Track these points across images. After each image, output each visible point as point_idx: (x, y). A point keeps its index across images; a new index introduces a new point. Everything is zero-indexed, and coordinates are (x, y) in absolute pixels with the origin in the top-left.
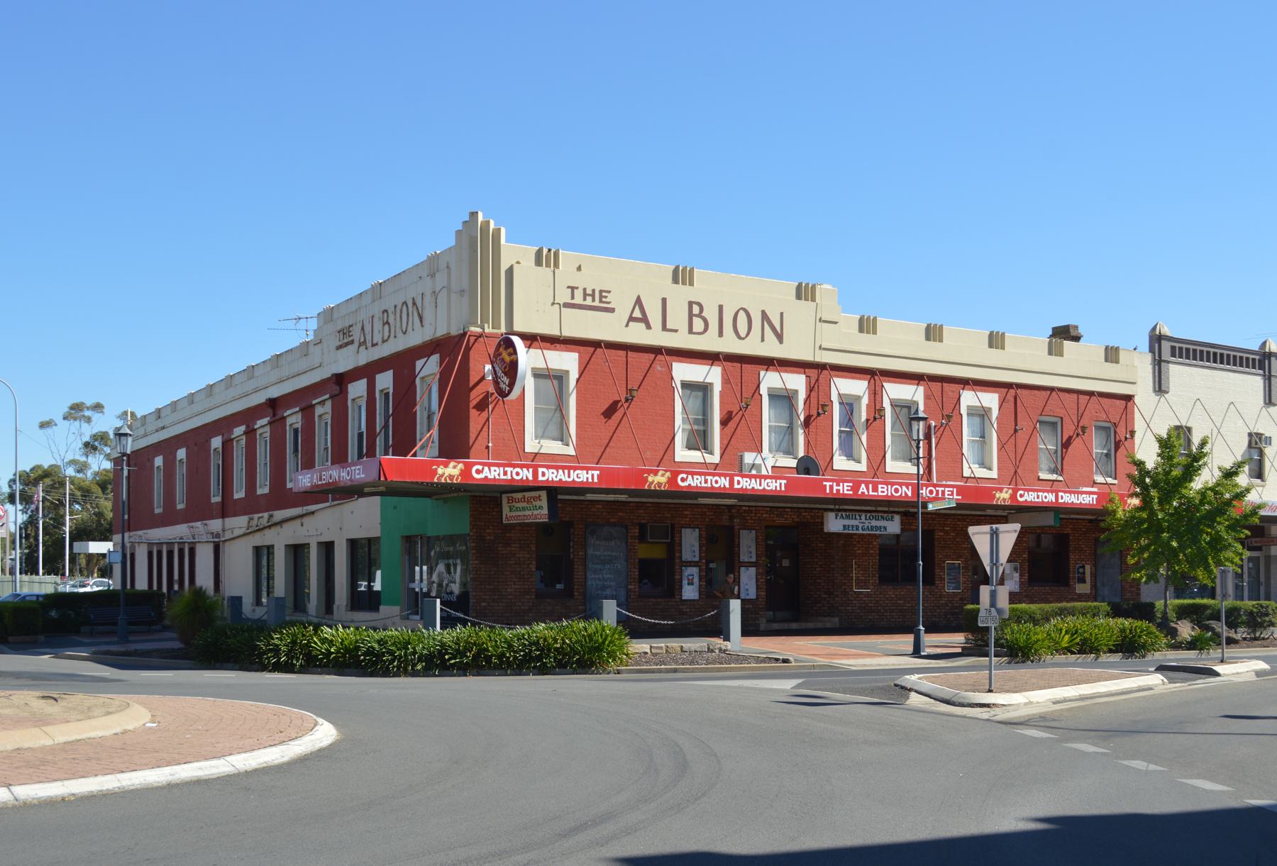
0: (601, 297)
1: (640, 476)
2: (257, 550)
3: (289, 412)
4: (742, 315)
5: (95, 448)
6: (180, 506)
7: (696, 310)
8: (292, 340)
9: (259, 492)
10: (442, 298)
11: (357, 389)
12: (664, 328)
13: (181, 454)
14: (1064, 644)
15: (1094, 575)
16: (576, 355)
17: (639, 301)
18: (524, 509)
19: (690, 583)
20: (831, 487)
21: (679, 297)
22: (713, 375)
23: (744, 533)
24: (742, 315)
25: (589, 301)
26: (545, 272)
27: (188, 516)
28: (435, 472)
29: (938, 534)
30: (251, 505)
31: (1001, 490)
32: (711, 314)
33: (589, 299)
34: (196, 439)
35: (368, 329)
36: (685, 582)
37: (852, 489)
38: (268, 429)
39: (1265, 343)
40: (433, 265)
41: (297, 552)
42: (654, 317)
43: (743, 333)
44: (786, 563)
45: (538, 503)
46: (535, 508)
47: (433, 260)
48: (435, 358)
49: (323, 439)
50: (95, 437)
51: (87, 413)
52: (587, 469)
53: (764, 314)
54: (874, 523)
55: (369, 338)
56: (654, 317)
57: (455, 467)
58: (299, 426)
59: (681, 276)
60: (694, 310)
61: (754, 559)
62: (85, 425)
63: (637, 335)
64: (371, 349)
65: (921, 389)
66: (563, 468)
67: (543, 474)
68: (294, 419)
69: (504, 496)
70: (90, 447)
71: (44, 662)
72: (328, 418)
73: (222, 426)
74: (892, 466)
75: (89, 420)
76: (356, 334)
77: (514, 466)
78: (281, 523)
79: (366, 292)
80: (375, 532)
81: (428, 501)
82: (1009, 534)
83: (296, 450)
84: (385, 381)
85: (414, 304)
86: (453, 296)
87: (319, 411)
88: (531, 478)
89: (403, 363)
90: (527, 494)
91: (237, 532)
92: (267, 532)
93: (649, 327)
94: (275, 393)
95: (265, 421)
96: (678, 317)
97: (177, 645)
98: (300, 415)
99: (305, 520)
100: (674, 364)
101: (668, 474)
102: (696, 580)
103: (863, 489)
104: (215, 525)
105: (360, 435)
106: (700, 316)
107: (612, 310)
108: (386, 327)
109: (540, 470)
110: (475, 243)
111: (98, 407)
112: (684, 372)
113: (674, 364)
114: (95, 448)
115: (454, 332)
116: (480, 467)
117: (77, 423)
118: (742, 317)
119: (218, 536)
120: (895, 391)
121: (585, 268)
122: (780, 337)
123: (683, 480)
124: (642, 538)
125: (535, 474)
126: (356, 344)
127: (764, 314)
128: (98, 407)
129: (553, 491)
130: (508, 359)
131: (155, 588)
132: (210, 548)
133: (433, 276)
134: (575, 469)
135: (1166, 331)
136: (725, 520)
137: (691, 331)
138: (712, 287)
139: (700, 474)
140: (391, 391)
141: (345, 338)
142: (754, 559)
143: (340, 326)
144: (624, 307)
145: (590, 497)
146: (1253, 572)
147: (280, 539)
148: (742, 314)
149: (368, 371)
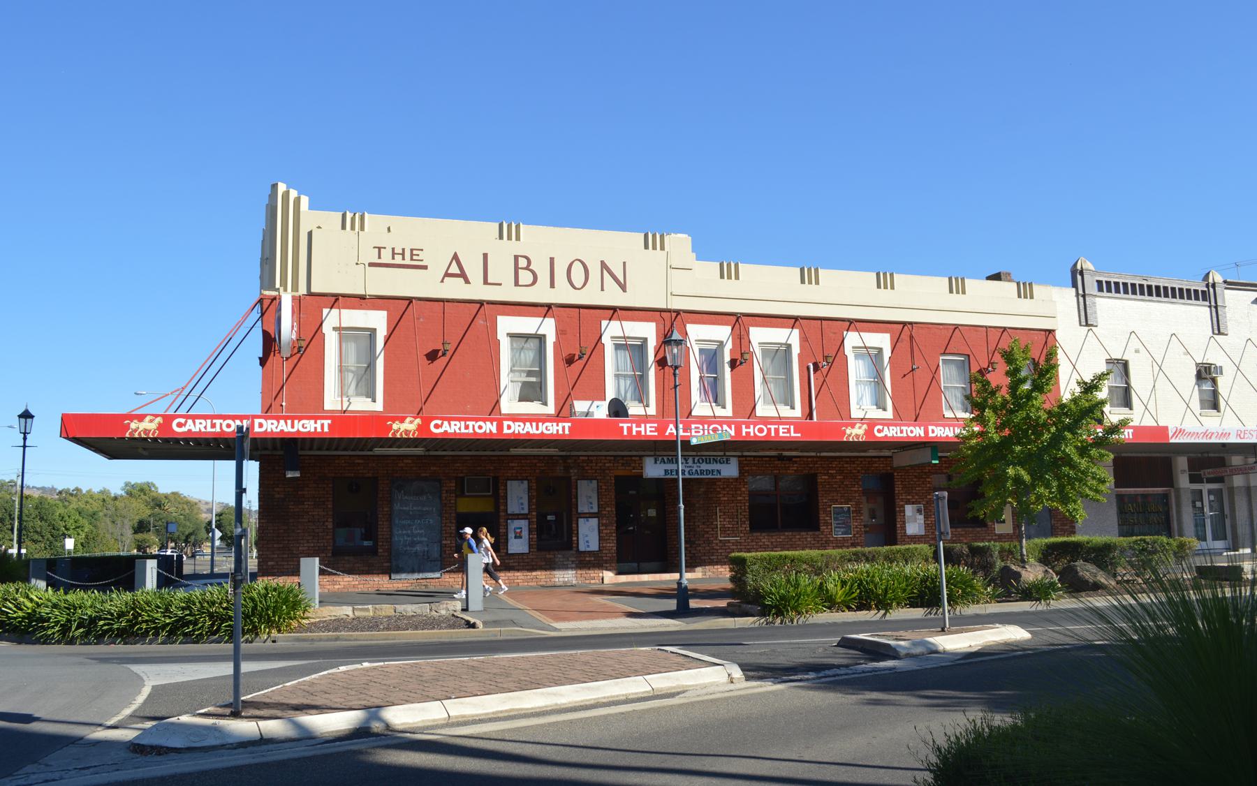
0: (412, 255)
1: (838, 429)
7: (523, 262)
12: (486, 282)
16: (384, 313)
17: (455, 257)
19: (518, 536)
20: (630, 429)
25: (398, 260)
28: (844, 432)
29: (822, 478)
31: (402, 420)
36: (511, 535)
42: (474, 269)
44: (652, 513)
53: (604, 265)
54: (704, 467)
57: (411, 422)
60: (521, 264)
61: (595, 510)
63: (454, 290)
65: (796, 332)
67: (509, 427)
71: (664, 586)
74: (763, 410)
77: (477, 420)
88: (494, 431)
93: (467, 281)
96: (501, 270)
100: (500, 318)
102: (525, 534)
106: (527, 268)
107: (425, 267)
109: (506, 423)
112: (507, 325)
113: (500, 318)
116: (439, 422)
118: (577, 268)
120: (759, 336)
123: (879, 431)
127: (604, 265)
134: (300, 419)
135: (1088, 265)
136: (559, 471)
137: (517, 284)
138: (539, 241)
139: (459, 420)
142: (595, 510)
144: (438, 261)
146: (1215, 505)
148: (577, 265)
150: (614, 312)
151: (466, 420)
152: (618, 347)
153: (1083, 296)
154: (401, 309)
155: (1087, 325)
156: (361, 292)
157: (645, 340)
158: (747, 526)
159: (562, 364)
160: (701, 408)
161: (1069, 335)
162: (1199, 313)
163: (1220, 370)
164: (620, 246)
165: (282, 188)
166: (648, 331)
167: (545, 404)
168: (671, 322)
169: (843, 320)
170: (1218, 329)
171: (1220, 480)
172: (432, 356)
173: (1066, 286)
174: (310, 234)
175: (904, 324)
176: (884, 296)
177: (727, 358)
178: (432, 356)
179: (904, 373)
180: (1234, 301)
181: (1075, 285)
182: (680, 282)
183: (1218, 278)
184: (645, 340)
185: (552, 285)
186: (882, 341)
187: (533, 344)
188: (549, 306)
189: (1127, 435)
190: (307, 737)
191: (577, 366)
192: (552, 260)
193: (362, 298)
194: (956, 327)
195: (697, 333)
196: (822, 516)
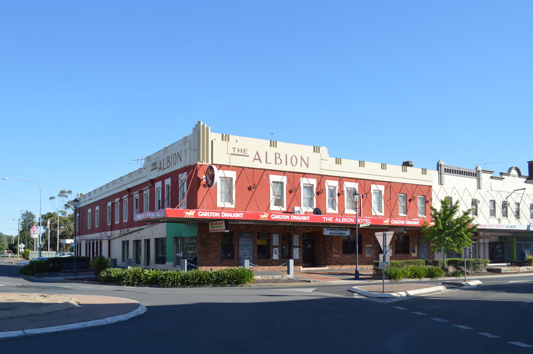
2: (123, 242)
5: (69, 206)
6: (97, 227)
7: (278, 156)
9: (124, 221)
11: (158, 185)
12: (266, 162)
13: (97, 208)
15: (418, 250)
17: (257, 153)
18: (216, 227)
21: (272, 151)
23: (295, 235)
24: (294, 157)
25: (240, 153)
27: (99, 230)
30: (121, 226)
31: (263, 214)
32: (283, 158)
33: (240, 152)
34: (102, 203)
35: (162, 163)
36: (274, 253)
37: (333, 219)
38: (127, 199)
41: (137, 243)
42: (263, 158)
45: (221, 225)
46: (221, 227)
47: (185, 138)
48: (185, 173)
49: (146, 202)
51: (66, 194)
53: (302, 158)
54: (341, 232)
55: (162, 167)
56: (263, 158)
58: (138, 198)
59: (273, 144)
60: (277, 156)
61: (298, 245)
62: (65, 198)
63: (257, 165)
64: (163, 171)
65: (357, 184)
66: (230, 212)
68: (136, 195)
69: (210, 223)
70: (67, 206)
72: (148, 195)
73: (111, 198)
75: (67, 196)
76: (158, 165)
77: (213, 212)
82: (390, 235)
83: (137, 207)
84: (168, 181)
86: (192, 151)
87: (145, 192)
89: (174, 175)
90: (218, 222)
91: (117, 236)
92: (127, 236)
93: (261, 162)
94: (129, 186)
95: (126, 196)
96: (271, 159)
98: (138, 194)
99: (140, 231)
101: (268, 215)
102: (278, 253)
103: (337, 220)
104: (109, 233)
105: (159, 201)
106: (279, 158)
107: (248, 156)
111: (70, 192)
112: (273, 178)
115: (192, 164)
118: (294, 158)
119: (110, 237)
121: (238, 141)
122: (307, 166)
123: (200, 214)
124: (259, 238)
125: (221, 215)
126: (158, 169)
127: (302, 158)
130: (211, 173)
133: (185, 144)
134: (235, 213)
135: (443, 163)
136: (288, 231)
137: (276, 163)
138: (283, 148)
141: (154, 166)
142: (298, 245)
143: (153, 162)
144: (252, 155)
145: (240, 223)
147: (131, 238)
148: (294, 157)
149: (162, 178)
150: (304, 175)
151: (210, 212)
152: (304, 187)
153: (440, 174)
154: (241, 170)
155: (441, 184)
157: (313, 185)
158: (341, 252)
159: (289, 194)
161: (436, 187)
163: (479, 202)
164: (306, 150)
165: (202, 122)
166: (313, 182)
167: (283, 207)
168: (321, 178)
169: (371, 180)
170: (479, 187)
171: (476, 240)
173: (434, 170)
174: (212, 142)
175: (389, 182)
176: (383, 172)
177: (337, 193)
178: (250, 189)
179: (388, 200)
180: (485, 177)
181: (438, 170)
182: (325, 165)
183: (480, 169)
184: (313, 185)
185: (286, 164)
186: (382, 188)
187: (279, 185)
188: (285, 172)
190: (408, 296)
191: (293, 194)
192: (286, 155)
193: (229, 166)
194: (404, 184)
196: (363, 249)
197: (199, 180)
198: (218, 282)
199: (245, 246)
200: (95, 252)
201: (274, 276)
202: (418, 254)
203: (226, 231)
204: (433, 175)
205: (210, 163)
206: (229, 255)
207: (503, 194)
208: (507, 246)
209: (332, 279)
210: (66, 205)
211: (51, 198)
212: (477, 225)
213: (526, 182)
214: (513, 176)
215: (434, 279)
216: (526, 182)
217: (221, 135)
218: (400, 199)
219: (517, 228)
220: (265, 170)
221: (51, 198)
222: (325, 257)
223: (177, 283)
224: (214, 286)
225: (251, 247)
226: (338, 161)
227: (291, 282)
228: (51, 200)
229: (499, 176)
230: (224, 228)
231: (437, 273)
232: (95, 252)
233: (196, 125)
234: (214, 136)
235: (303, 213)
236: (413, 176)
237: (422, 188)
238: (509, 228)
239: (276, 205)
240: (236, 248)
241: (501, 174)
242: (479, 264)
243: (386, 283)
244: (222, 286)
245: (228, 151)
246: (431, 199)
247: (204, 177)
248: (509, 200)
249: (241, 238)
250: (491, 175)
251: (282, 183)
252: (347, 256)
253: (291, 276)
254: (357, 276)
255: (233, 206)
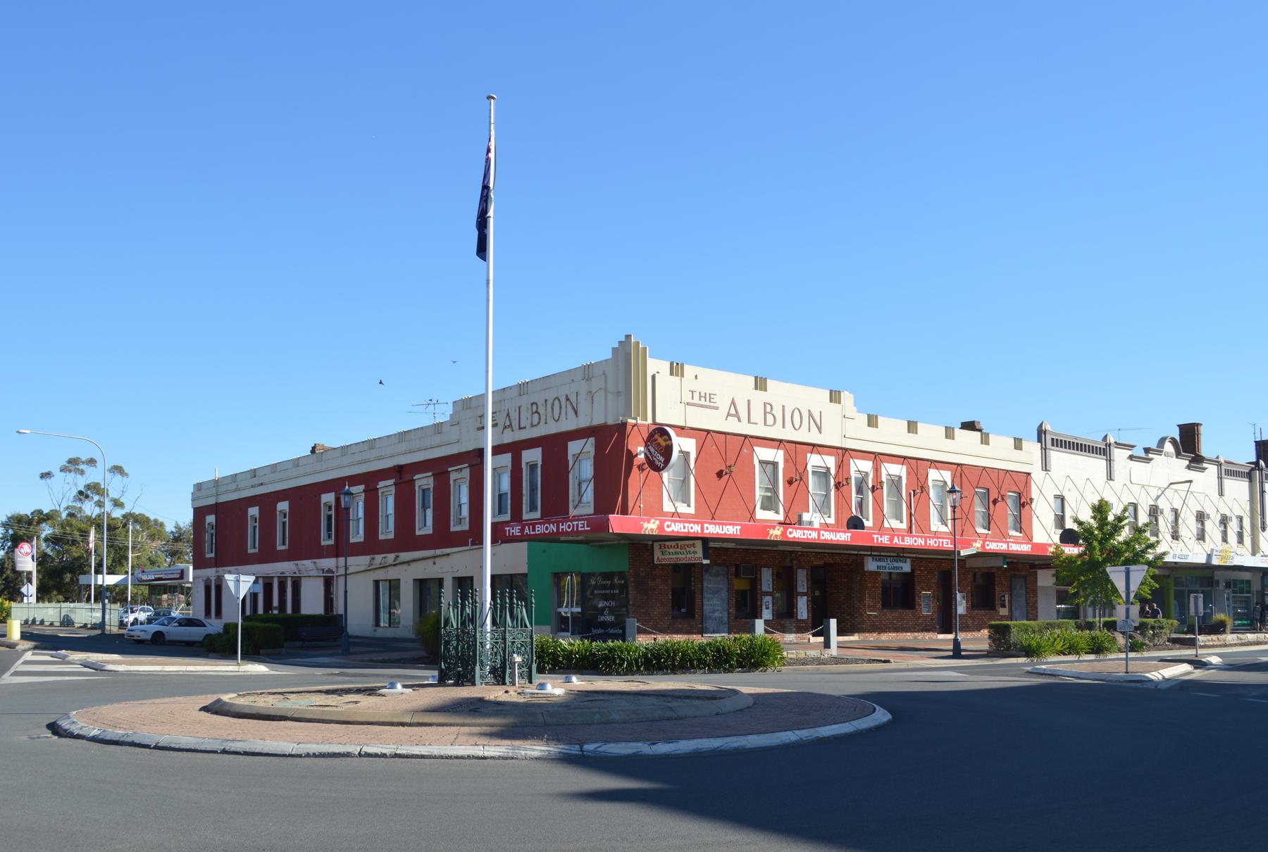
3: (417, 476)
4: (797, 412)
5: (87, 497)
7: (768, 408)
8: (427, 421)
10: (599, 398)
13: (283, 506)
14: (1059, 648)
15: (1010, 602)
17: (733, 403)
21: (758, 397)
22: (778, 456)
23: (799, 571)
24: (797, 412)
25: (702, 402)
26: (676, 379)
27: (290, 556)
30: (371, 545)
35: (514, 415)
39: (1041, 425)
40: (587, 372)
42: (743, 414)
43: (797, 426)
45: (692, 549)
47: (587, 368)
48: (592, 440)
50: (88, 487)
51: (82, 467)
52: (734, 525)
53: (810, 415)
54: (896, 564)
55: (515, 423)
56: (743, 414)
59: (760, 384)
60: (768, 408)
62: (79, 476)
69: (656, 546)
70: (82, 496)
75: (82, 472)
78: (408, 563)
79: (510, 388)
80: (523, 569)
81: (584, 547)
82: (1139, 574)
85: (568, 399)
86: (610, 396)
90: (680, 543)
93: (739, 420)
95: (391, 482)
96: (757, 415)
97: (422, 653)
98: (431, 479)
99: (437, 560)
103: (527, 531)
104: (328, 563)
107: (717, 408)
108: (536, 416)
110: (626, 357)
111: (92, 462)
112: (764, 453)
114: (87, 497)
115: (611, 421)
117: (73, 474)
118: (797, 414)
119: (330, 571)
121: (700, 378)
122: (820, 429)
124: (737, 575)
125: (702, 529)
127: (810, 415)
128: (92, 462)
129: (705, 541)
130: (663, 444)
131: (289, 611)
132: (320, 585)
133: (589, 379)
135: (1048, 428)
136: (788, 563)
138: (781, 393)
140: (540, 463)
144: (724, 406)
145: (781, 548)
150: (815, 448)
153: (1044, 449)
156: (683, 424)
158: (879, 606)
160: (935, 525)
161: (1037, 474)
162: (1099, 463)
164: (816, 398)
166: (830, 462)
167: (777, 512)
170: (1110, 477)
172: (720, 475)
174: (653, 377)
180: (1119, 455)
181: (1039, 440)
183: (1111, 440)
186: (947, 476)
188: (781, 441)
189: (1168, 559)
194: (984, 468)
195: (933, 475)
197: (631, 456)
198: (720, 664)
199: (714, 593)
200: (276, 603)
201: (808, 652)
202: (1011, 610)
203: (706, 562)
204: (1032, 449)
205: (650, 421)
206: (685, 611)
207: (1150, 490)
208: (1191, 596)
209: (914, 659)
210: (81, 493)
211: (46, 476)
212: (1164, 554)
213: (1189, 467)
214: (1167, 455)
215: (1101, 657)
216: (1189, 467)
217: (668, 364)
218: (977, 500)
219: (1189, 560)
220: (746, 436)
221: (46, 476)
222: (852, 616)
223: (638, 668)
224: (711, 671)
225: (724, 594)
226: (872, 421)
227: (922, 662)
228: (43, 481)
229: (1143, 454)
230: (700, 554)
231: (1106, 645)
232: (276, 603)
233: (620, 342)
234: (656, 366)
235: (819, 525)
236: (997, 454)
237: (994, 476)
238: (1177, 560)
239: (763, 508)
240: (698, 596)
241: (1147, 450)
242: (1162, 628)
243: (1132, 659)
244: (727, 671)
245: (686, 397)
246: (1031, 500)
247: (641, 449)
248: (1162, 504)
249: (706, 577)
250: (1130, 453)
251: (775, 464)
252: (890, 614)
253: (834, 651)
254: (957, 653)
255: (692, 510)
